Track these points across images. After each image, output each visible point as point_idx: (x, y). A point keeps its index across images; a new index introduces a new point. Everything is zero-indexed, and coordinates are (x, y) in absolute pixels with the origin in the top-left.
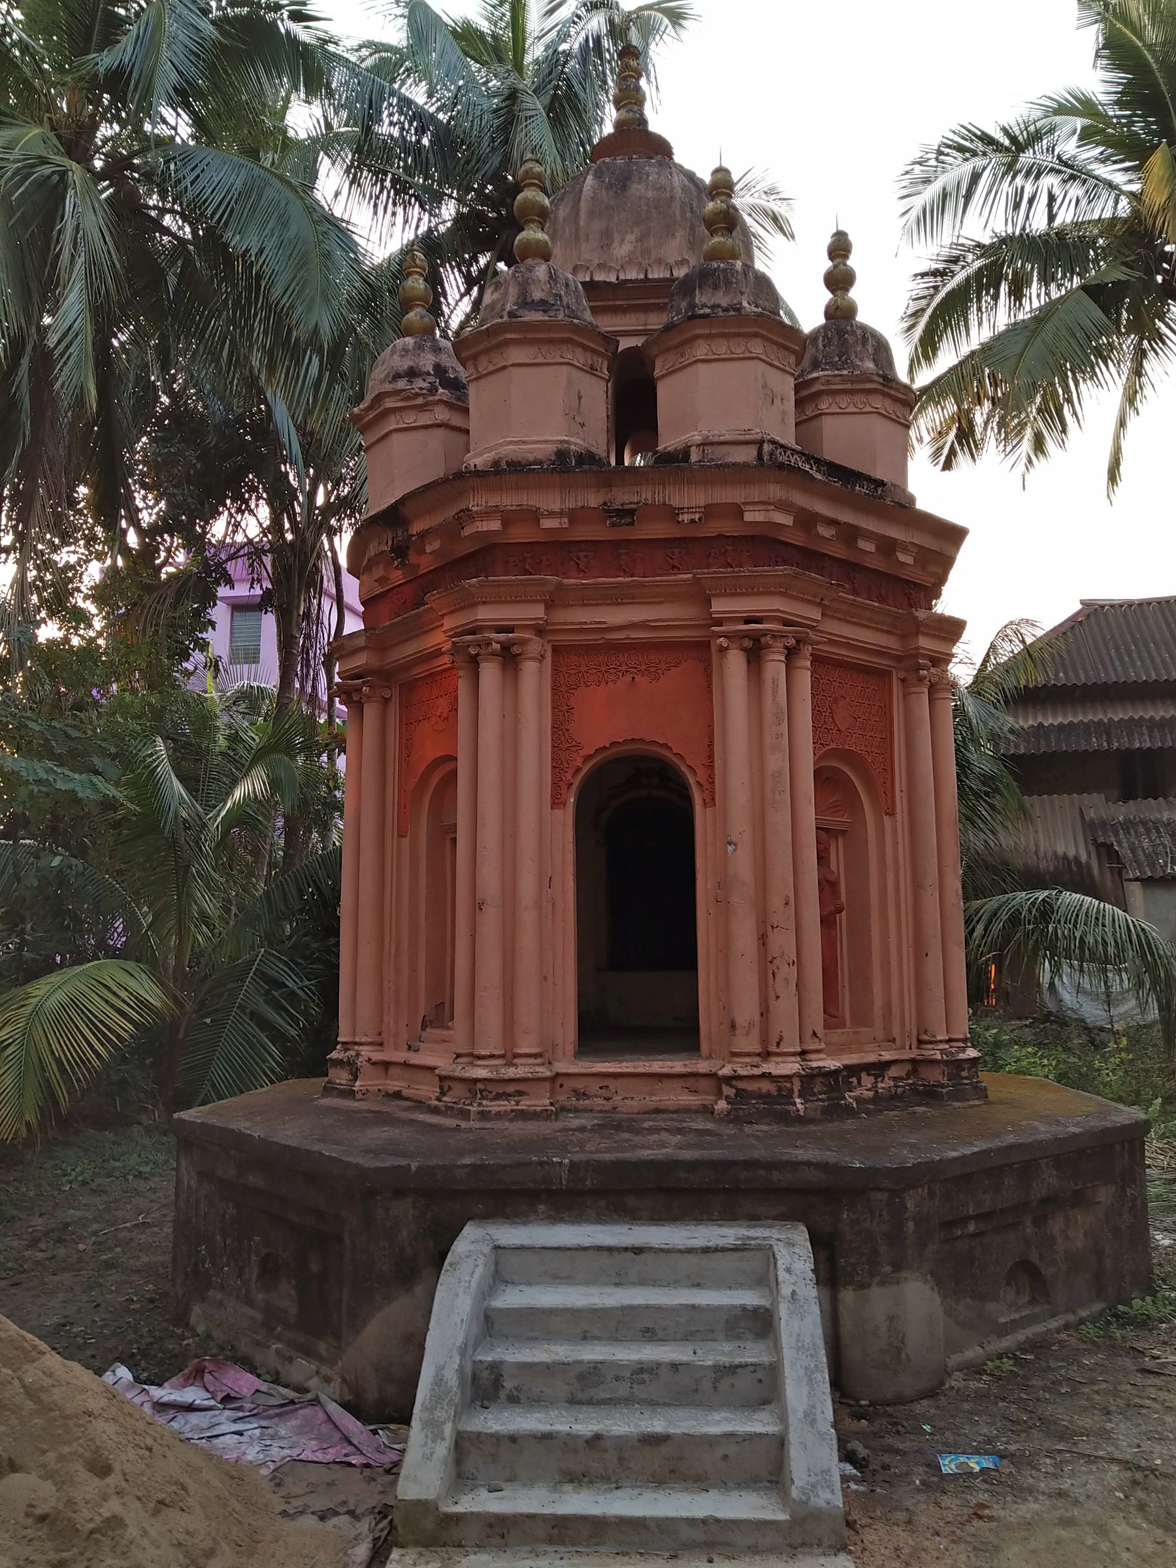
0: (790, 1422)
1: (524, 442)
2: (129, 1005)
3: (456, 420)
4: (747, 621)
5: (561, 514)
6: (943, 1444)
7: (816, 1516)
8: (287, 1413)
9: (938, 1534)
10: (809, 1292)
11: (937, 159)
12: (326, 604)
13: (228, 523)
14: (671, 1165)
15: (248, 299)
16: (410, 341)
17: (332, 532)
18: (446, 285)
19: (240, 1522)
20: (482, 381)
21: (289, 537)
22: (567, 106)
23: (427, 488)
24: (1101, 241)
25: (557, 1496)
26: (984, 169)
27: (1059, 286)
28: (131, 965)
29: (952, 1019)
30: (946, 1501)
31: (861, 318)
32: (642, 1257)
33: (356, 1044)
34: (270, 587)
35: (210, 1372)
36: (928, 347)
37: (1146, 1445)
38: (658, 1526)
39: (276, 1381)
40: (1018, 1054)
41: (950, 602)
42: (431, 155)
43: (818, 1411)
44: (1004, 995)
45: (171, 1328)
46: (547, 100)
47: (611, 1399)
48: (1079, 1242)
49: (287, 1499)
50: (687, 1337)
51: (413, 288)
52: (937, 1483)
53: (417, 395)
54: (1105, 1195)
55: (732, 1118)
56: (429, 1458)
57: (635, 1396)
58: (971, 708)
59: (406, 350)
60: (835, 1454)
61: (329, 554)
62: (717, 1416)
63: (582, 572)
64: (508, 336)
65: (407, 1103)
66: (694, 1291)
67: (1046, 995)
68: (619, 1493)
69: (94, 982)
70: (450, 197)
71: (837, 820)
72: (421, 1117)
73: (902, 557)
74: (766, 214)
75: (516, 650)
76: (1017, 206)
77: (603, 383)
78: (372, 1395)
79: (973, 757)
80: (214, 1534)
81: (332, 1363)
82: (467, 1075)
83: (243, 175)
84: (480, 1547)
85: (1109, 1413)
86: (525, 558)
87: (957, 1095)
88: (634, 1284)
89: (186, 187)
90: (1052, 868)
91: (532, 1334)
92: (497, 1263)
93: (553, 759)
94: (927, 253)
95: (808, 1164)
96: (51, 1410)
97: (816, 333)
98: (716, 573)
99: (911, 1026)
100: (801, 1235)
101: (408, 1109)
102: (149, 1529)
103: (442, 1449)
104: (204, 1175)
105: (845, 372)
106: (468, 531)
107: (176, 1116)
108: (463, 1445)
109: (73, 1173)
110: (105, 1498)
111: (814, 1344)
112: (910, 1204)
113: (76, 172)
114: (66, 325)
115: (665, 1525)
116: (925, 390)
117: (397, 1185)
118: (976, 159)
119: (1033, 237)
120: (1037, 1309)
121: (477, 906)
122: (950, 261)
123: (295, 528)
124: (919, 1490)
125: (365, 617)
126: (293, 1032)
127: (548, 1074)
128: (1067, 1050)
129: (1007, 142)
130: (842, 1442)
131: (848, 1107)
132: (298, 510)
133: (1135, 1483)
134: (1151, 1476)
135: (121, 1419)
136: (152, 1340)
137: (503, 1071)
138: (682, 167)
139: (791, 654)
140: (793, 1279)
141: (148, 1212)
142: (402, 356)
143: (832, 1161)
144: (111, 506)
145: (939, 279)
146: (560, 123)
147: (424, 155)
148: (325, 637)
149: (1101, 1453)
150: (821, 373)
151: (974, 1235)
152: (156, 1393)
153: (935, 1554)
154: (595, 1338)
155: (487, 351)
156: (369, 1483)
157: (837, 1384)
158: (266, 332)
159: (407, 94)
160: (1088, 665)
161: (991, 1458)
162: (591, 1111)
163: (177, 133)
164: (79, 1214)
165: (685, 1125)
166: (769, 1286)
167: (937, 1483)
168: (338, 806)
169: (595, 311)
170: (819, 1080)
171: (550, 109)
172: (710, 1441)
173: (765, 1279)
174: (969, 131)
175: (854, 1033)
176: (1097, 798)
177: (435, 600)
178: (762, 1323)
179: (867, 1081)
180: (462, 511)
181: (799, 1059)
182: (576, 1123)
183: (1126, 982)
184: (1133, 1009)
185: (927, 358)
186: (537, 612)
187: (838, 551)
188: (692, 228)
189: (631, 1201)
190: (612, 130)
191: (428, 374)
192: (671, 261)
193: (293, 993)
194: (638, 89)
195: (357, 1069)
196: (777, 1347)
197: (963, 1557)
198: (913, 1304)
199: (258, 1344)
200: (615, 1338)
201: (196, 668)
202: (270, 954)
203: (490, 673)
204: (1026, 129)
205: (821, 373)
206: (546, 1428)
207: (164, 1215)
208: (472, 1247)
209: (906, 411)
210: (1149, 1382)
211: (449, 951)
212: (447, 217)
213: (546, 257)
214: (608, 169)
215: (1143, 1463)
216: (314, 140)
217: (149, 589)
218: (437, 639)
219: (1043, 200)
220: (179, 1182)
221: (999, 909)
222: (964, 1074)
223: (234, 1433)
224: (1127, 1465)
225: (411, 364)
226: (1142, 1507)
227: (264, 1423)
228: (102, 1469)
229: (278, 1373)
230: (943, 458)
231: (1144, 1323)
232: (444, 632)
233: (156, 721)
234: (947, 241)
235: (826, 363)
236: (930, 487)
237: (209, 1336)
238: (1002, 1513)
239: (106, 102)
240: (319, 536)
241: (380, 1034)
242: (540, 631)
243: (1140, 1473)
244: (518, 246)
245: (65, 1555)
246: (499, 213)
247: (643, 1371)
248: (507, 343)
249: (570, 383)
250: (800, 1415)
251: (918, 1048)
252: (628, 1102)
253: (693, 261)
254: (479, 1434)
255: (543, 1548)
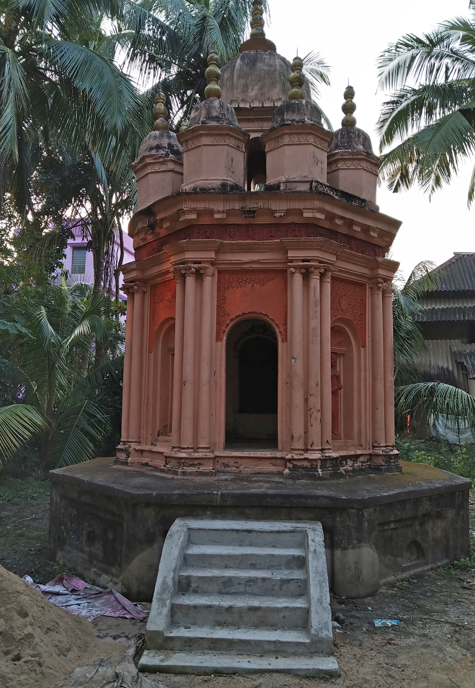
0: (312, 602)
1: (207, 180)
2: (28, 424)
3: (177, 169)
4: (303, 261)
5: (223, 212)
6: (376, 615)
7: (321, 641)
8: (98, 597)
9: (372, 650)
10: (322, 550)
11: (396, 50)
12: (116, 247)
13: (73, 210)
14: (264, 496)
15: (85, 110)
16: (157, 133)
17: (119, 215)
18: (172, 104)
19: (80, 639)
20: (189, 152)
21: (100, 217)
22: (228, 23)
23: (164, 199)
24: (469, 89)
25: (213, 631)
26: (417, 54)
27: (449, 109)
28: (29, 407)
29: (388, 437)
30: (376, 637)
31: (358, 126)
32: (251, 534)
33: (129, 442)
34: (91, 240)
35: (66, 580)
36: (388, 137)
37: (461, 617)
38: (255, 644)
39: (94, 584)
40: (418, 454)
41: (394, 253)
42: (166, 44)
43: (324, 598)
44: (413, 429)
45: (48, 562)
46: (219, 20)
47: (236, 592)
48: (439, 533)
49: (99, 630)
50: (269, 568)
51: (159, 109)
52: (373, 630)
53: (160, 157)
54: (450, 514)
55: (291, 477)
56: (160, 614)
57: (247, 583)
58: (402, 301)
59: (155, 137)
60: (330, 616)
61: (117, 225)
62: (281, 600)
63: (232, 238)
64: (201, 132)
65: (151, 468)
66: (273, 549)
67: (432, 429)
68: (239, 630)
69: (13, 414)
70: (175, 63)
71: (340, 349)
72: (157, 474)
73: (372, 234)
74: (318, 73)
75: (202, 271)
76: (431, 72)
77: (242, 154)
78: (135, 590)
79: (403, 322)
80: (70, 643)
81: (118, 577)
82: (177, 456)
83: (83, 54)
84: (181, 650)
85: (447, 604)
86: (207, 231)
87: (389, 470)
88: (248, 546)
89: (57, 61)
90: (436, 373)
91: (203, 565)
92: (189, 536)
93: (217, 320)
94: (389, 93)
95: (323, 497)
96: (3, 590)
97: (338, 132)
98: (290, 239)
99: (370, 440)
100: (319, 527)
101: (151, 470)
102: (44, 639)
103: (166, 611)
104: (63, 497)
105: (350, 150)
106: (182, 219)
107: (51, 471)
108: (174, 609)
109: (4, 496)
110: (26, 626)
111: (323, 571)
112: (366, 515)
113: (10, 54)
114: (5, 123)
115: (259, 643)
116: (386, 156)
117: (148, 502)
118: (413, 50)
119: (438, 87)
120: (420, 561)
121: (183, 383)
122: (400, 97)
123: (102, 213)
124: (365, 633)
125: (136, 255)
126: (99, 437)
127: (212, 456)
128: (440, 453)
129: (428, 42)
130: (333, 613)
131: (341, 473)
132: (104, 205)
133: (456, 631)
134: (463, 629)
135: (31, 595)
136: (40, 566)
137: (193, 454)
138: (280, 55)
139: (322, 276)
140: (315, 544)
141: (37, 513)
142: (154, 139)
143: (333, 495)
144: (22, 203)
145: (395, 105)
146: (225, 31)
147: (163, 43)
148: (115, 263)
149: (442, 620)
150: (340, 151)
151: (393, 529)
152: (43, 587)
153: (370, 658)
154: (231, 567)
155: (191, 139)
156: (134, 625)
157: (332, 590)
158: (92, 124)
159: (156, 16)
160: (456, 282)
161: (396, 621)
162: (230, 472)
163: (52, 33)
164: (7, 513)
165: (270, 479)
166: (304, 547)
167: (373, 630)
168: (122, 339)
169: (239, 120)
170: (329, 461)
171: (221, 25)
172: (278, 610)
173: (303, 545)
174: (411, 37)
175: (345, 442)
176: (458, 342)
177: (166, 249)
178: (301, 562)
179: (350, 463)
180: (180, 209)
181: (320, 452)
182: (223, 477)
183: (467, 424)
184: (470, 436)
185: (388, 142)
186: (212, 255)
187: (344, 231)
188: (284, 84)
189: (247, 511)
190: (249, 38)
191: (165, 147)
192: (274, 99)
193: (99, 420)
194: (261, 19)
195: (129, 453)
196: (307, 572)
197: (382, 659)
198: (366, 556)
199: (86, 568)
200: (239, 567)
201: (57, 275)
202: (89, 403)
203: (190, 281)
204: (437, 36)
205: (340, 151)
206: (209, 603)
207: (44, 515)
208: (179, 528)
209: (376, 168)
210: (465, 592)
211: (170, 402)
212: (173, 73)
213: (219, 97)
214: (247, 56)
215: (460, 624)
216: (113, 37)
217: (38, 240)
218: (167, 266)
219: (444, 69)
220: (52, 500)
221: (412, 390)
222: (392, 461)
223: (76, 604)
224: (452, 624)
225: (158, 143)
226: (458, 641)
227: (89, 601)
228: (24, 615)
229: (94, 581)
230: (394, 187)
231: (465, 568)
232: (171, 263)
233: (41, 298)
234: (399, 88)
235: (342, 146)
236: (387, 201)
237: (64, 565)
238: (399, 642)
239: (22, 20)
240: (113, 217)
241: (139, 438)
242: (213, 263)
243: (458, 628)
244: (206, 91)
245: (9, 648)
246: (197, 71)
247: (251, 581)
248: (201, 135)
249: (228, 154)
250: (316, 600)
251: (372, 449)
252: (246, 469)
253: (284, 99)
254: (181, 605)
255: (207, 651)
